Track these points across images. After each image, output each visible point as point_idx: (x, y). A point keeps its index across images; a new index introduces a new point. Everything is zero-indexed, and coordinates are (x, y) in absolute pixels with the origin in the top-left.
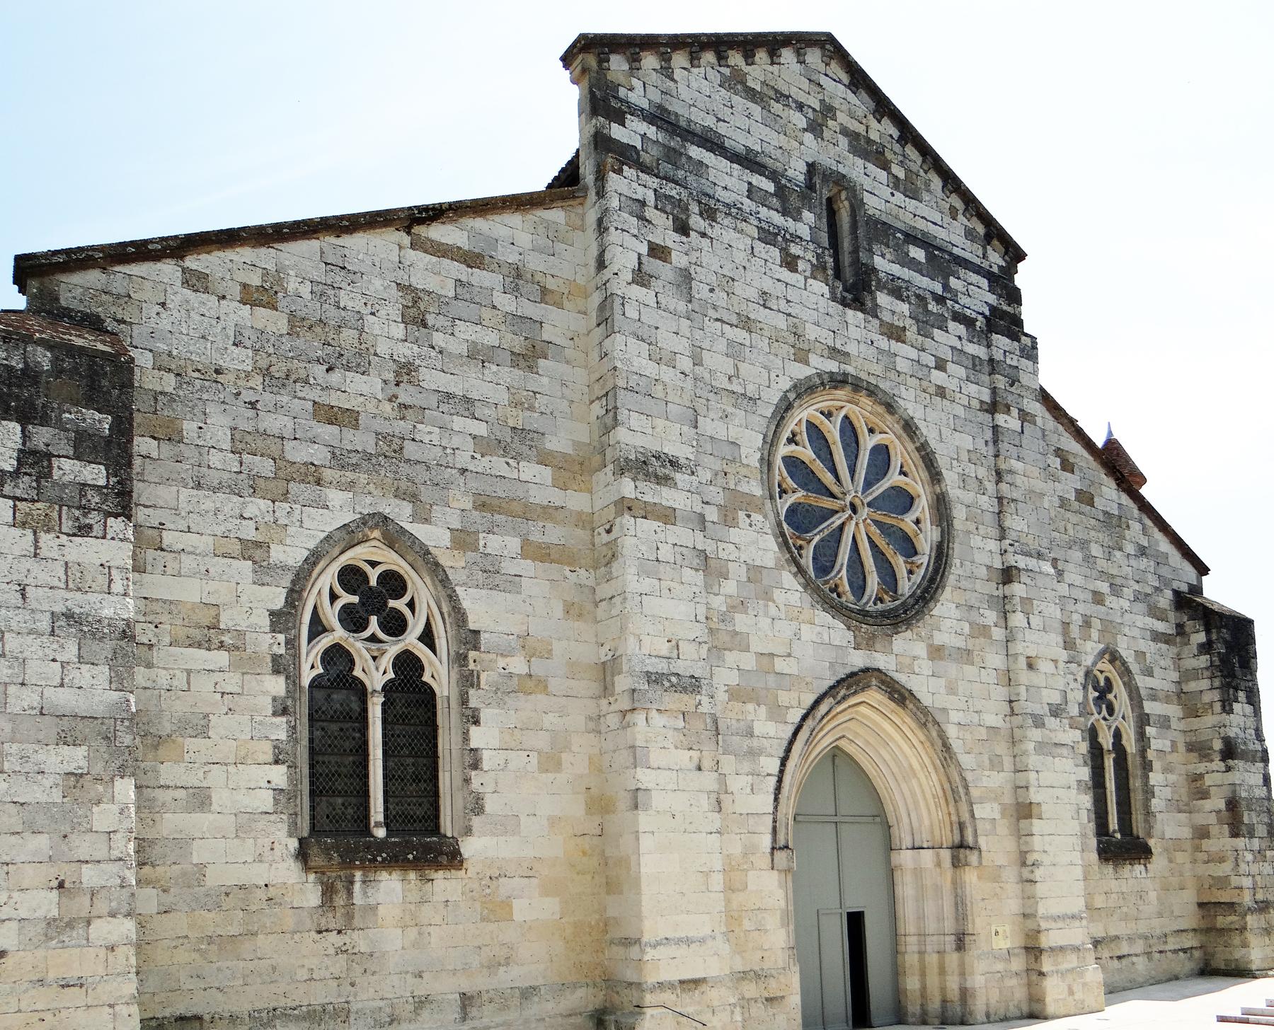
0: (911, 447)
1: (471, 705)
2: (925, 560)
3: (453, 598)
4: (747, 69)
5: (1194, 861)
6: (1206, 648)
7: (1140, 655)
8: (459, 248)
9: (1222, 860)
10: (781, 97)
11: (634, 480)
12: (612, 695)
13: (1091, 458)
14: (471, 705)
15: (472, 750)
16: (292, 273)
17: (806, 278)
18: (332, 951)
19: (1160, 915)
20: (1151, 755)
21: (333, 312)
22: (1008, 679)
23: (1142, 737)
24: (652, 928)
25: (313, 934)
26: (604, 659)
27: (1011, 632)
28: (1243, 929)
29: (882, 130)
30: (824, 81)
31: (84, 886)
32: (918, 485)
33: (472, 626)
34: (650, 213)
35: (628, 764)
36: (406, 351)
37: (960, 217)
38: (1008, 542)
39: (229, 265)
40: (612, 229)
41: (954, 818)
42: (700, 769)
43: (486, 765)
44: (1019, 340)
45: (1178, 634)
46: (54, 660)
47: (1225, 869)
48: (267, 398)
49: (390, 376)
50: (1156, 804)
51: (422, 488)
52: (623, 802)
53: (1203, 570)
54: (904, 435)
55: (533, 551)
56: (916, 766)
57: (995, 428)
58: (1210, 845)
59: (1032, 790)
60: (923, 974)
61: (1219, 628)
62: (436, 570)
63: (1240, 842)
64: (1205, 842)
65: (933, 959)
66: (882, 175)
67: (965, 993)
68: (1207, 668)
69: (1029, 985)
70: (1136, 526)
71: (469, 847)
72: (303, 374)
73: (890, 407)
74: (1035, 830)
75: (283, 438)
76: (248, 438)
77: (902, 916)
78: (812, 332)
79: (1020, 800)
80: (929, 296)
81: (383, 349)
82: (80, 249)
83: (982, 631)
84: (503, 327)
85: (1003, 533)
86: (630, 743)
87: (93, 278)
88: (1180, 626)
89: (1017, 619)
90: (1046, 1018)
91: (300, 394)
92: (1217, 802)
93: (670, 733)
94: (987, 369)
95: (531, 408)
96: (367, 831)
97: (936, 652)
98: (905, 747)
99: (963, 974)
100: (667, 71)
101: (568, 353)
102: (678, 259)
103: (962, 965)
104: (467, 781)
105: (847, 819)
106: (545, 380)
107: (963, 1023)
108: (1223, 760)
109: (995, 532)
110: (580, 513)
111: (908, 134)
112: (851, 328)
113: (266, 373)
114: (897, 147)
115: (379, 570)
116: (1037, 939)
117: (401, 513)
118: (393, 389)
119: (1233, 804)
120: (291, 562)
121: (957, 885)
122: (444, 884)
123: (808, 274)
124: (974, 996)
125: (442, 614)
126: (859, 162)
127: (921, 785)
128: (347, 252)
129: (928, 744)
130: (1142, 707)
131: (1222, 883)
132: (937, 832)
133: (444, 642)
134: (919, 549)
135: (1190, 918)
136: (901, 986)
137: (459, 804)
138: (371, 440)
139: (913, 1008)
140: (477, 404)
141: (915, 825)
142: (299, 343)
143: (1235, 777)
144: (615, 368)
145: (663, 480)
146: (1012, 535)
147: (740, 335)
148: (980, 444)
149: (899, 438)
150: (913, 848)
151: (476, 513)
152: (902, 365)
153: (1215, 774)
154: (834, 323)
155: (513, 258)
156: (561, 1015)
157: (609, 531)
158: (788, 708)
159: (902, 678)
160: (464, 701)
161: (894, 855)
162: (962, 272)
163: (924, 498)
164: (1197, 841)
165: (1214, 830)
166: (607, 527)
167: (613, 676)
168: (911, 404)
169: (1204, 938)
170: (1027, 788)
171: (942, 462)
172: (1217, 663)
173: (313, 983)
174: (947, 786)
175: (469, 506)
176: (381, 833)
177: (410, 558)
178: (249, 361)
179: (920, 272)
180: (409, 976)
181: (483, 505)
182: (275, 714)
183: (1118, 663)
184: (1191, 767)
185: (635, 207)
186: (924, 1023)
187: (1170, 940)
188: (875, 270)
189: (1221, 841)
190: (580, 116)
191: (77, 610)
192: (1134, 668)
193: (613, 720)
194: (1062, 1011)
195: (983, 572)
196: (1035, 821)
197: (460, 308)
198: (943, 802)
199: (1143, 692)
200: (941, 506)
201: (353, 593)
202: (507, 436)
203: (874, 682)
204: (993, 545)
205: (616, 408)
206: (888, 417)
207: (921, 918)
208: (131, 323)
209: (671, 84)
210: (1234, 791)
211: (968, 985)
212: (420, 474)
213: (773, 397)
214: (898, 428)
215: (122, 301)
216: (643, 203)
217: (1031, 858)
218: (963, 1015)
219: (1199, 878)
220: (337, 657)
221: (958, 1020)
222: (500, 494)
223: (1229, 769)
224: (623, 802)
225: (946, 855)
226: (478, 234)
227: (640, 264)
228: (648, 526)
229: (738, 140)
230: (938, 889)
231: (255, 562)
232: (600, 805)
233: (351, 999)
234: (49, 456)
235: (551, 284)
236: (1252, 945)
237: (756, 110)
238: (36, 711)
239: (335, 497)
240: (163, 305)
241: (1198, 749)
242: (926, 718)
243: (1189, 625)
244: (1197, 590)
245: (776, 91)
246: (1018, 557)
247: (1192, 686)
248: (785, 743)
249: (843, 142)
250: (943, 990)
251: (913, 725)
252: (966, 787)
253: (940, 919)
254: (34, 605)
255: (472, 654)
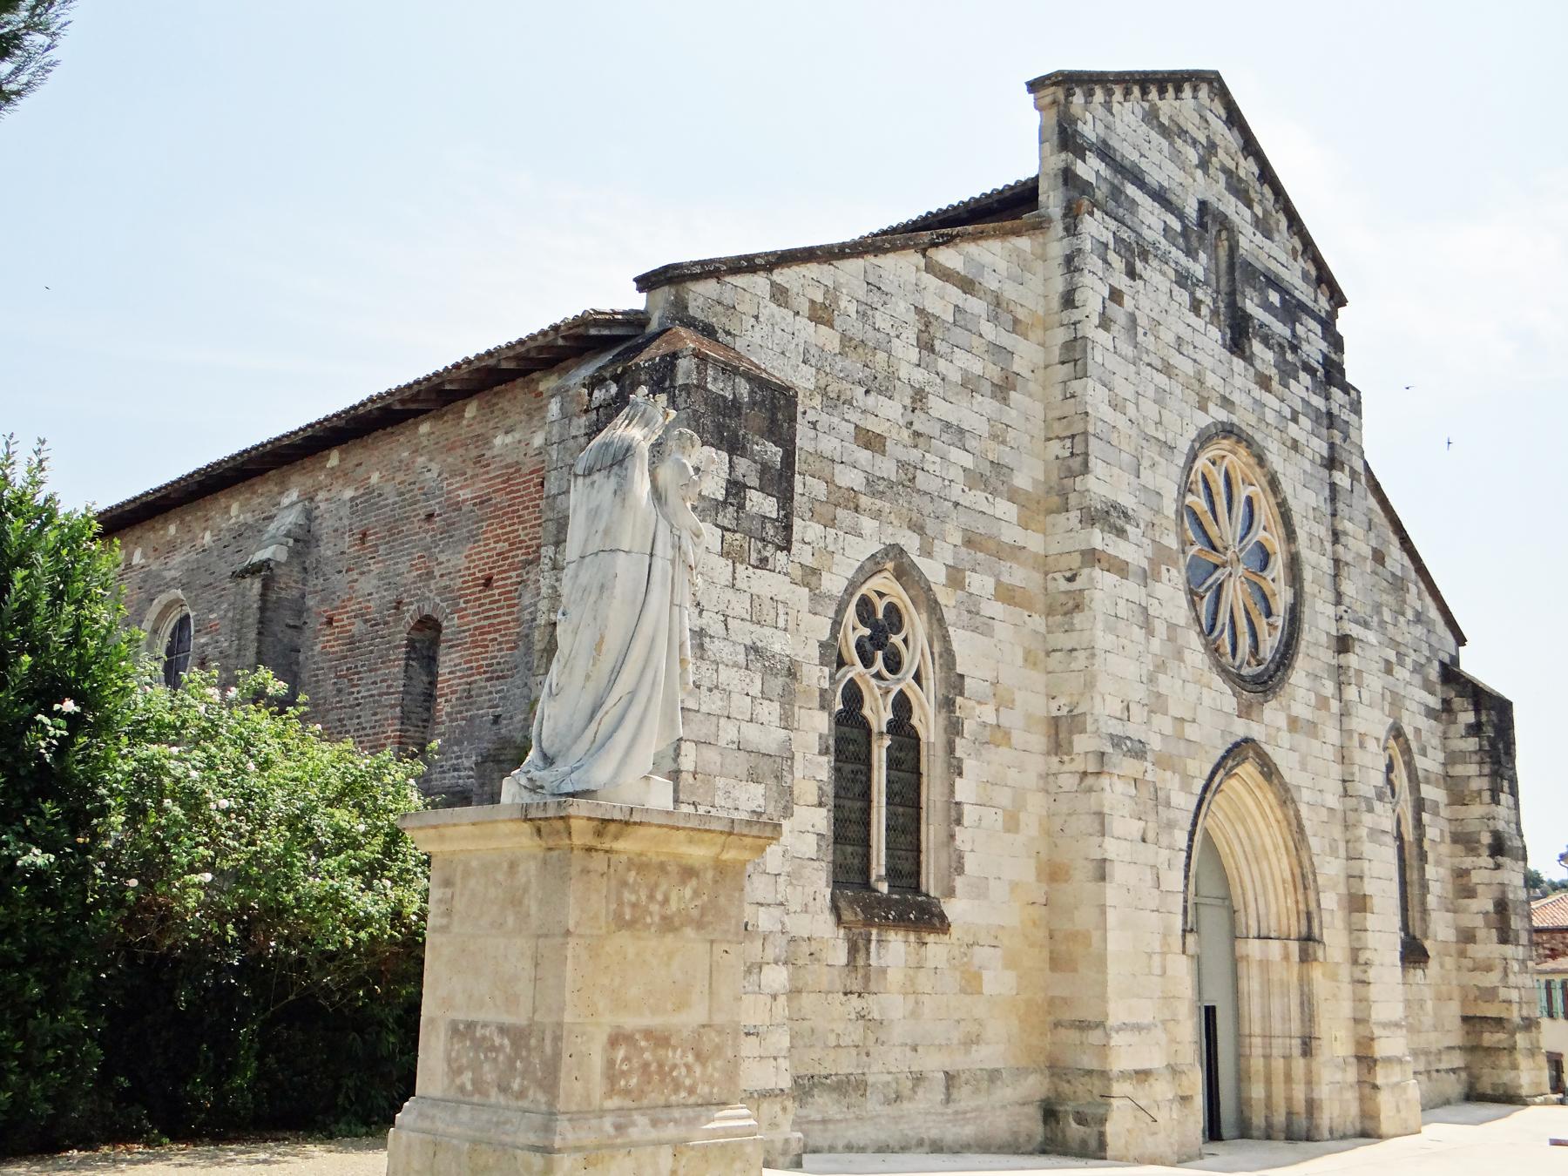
0: (1272, 501)
1: (957, 755)
2: (1280, 623)
3: (946, 639)
4: (1160, 103)
5: (1459, 968)
6: (1475, 729)
7: (1418, 731)
8: (958, 273)
9: (1489, 969)
10: (1183, 133)
11: (1102, 531)
12: (1069, 753)
13: (1382, 514)
14: (957, 755)
15: (956, 803)
16: (844, 291)
17: (1206, 323)
18: (853, 1016)
19: (1435, 1028)
20: (1427, 845)
21: (871, 333)
22: (1343, 758)
23: (1419, 824)
24: (1117, 1013)
25: (841, 994)
26: (1055, 713)
27: (1346, 705)
28: (1512, 1049)
29: (1248, 168)
30: (1210, 116)
31: (760, 929)
32: (1276, 544)
33: (959, 670)
34: (1112, 257)
35: (1091, 831)
36: (919, 376)
37: (1299, 258)
38: (1343, 608)
39: (802, 281)
40: (1086, 272)
41: (1302, 907)
42: (1144, 840)
43: (966, 821)
44: (1349, 394)
45: (1444, 710)
46: (747, 694)
47: (1492, 979)
48: (824, 419)
49: (908, 402)
50: (1431, 900)
51: (928, 520)
52: (1082, 872)
53: (1461, 640)
54: (1268, 489)
55: (1006, 594)
56: (1270, 847)
57: (1333, 486)
58: (1473, 950)
59: (1366, 880)
60: (1268, 1081)
61: (1488, 709)
62: (933, 608)
63: (1509, 950)
64: (1470, 947)
65: (1278, 1065)
66: (1247, 213)
67: (1311, 1105)
68: (1475, 752)
69: (1362, 1099)
70: (1413, 589)
71: (953, 909)
72: (848, 395)
73: (1261, 461)
74: (1369, 925)
75: (833, 461)
76: (811, 459)
77: (1246, 1014)
78: (1212, 380)
79: (1353, 891)
80: (1286, 344)
81: (903, 374)
82: (712, 261)
83: (1323, 703)
84: (986, 357)
85: (1339, 599)
86: (1094, 808)
87: (708, 288)
88: (1446, 703)
89: (1351, 693)
90: (1380, 1137)
91: (847, 417)
92: (1485, 903)
93: (1128, 801)
94: (1325, 422)
95: (1004, 442)
96: (867, 885)
97: (1293, 723)
98: (1262, 825)
99: (1309, 1083)
100: (1108, 106)
101: (1032, 386)
102: (1128, 302)
103: (1309, 1071)
104: (952, 837)
105: (1208, 901)
106: (1014, 413)
107: (1309, 1139)
108: (1492, 855)
109: (1331, 596)
110: (1036, 555)
111: (1267, 174)
112: (1236, 376)
113: (824, 391)
114: (1257, 185)
115: (886, 600)
116: (1370, 1047)
117: (910, 542)
118: (910, 416)
119: (1502, 906)
120: (835, 592)
121: (1305, 984)
122: (937, 948)
123: (1207, 319)
124: (1320, 1108)
125: (932, 653)
126: (1233, 199)
127: (1271, 868)
128: (881, 272)
129: (1284, 824)
130: (1419, 790)
131: (1489, 994)
132: (1284, 921)
133: (932, 683)
134: (1274, 610)
135: (1455, 1035)
136: (1244, 1095)
137: (944, 861)
138: (893, 466)
139: (1258, 1120)
140: (967, 435)
141: (1262, 911)
142: (847, 363)
143: (1501, 876)
144: (1086, 413)
145: (1121, 533)
146: (1346, 600)
147: (1161, 379)
148: (1322, 504)
149: (1264, 491)
150: (1259, 937)
151: (964, 549)
152: (1270, 417)
153: (1483, 871)
154: (1223, 370)
155: (994, 286)
156: (1017, 1103)
157: (1071, 579)
158: (1193, 777)
159: (1268, 749)
160: (951, 748)
161: (1240, 944)
162: (1305, 318)
163: (1279, 555)
164: (1462, 946)
165: (1481, 934)
166: (1068, 574)
167: (1071, 733)
168: (1275, 459)
169: (1469, 1058)
170: (1361, 878)
171: (1297, 519)
172: (1487, 748)
173: (840, 1050)
174: (1297, 871)
175: (959, 541)
176: (884, 888)
177: (913, 592)
178: (813, 380)
179: (1275, 316)
180: (908, 1049)
181: (969, 542)
182: (820, 753)
183: (1401, 739)
184: (1456, 861)
185: (1102, 249)
186: (1269, 1137)
187: (1444, 1057)
188: (1250, 317)
189: (1487, 947)
190: (1041, 142)
191: (759, 644)
192: (1414, 746)
193: (1068, 782)
194: (1392, 1132)
195: (1323, 639)
196: (1369, 915)
197: (959, 335)
198: (1291, 889)
199: (1421, 774)
200: (1294, 563)
202: (986, 469)
203: (1251, 754)
204: (1330, 610)
205: (1086, 454)
206: (1258, 469)
207: (1267, 1016)
208: (735, 335)
209: (1111, 118)
210: (1504, 893)
211: (1315, 1096)
212: (928, 508)
213: (1184, 446)
214: (1264, 481)
215: (729, 313)
216: (1106, 246)
217: (1362, 958)
218: (1309, 1130)
219: (1462, 987)
221: (1304, 1134)
222: (982, 531)
223: (1498, 867)
224: (1082, 872)
225: (1294, 947)
226: (969, 260)
227: (1104, 307)
228: (1110, 579)
229: (1155, 177)
230: (1284, 985)
231: (811, 590)
232: (1054, 873)
233: (866, 1070)
234: (745, 486)
235: (1021, 314)
236: (1521, 1067)
237: (1165, 144)
238: (735, 746)
239: (868, 524)
240: (756, 317)
241: (1464, 840)
242: (1286, 797)
243: (1458, 702)
244: (1455, 660)
245: (1179, 127)
246: (1353, 625)
247: (1459, 770)
248: (1191, 816)
249: (1222, 178)
250: (1289, 1100)
251: (1274, 802)
252: (1314, 874)
253: (1286, 1019)
254: (733, 638)
255: (959, 700)
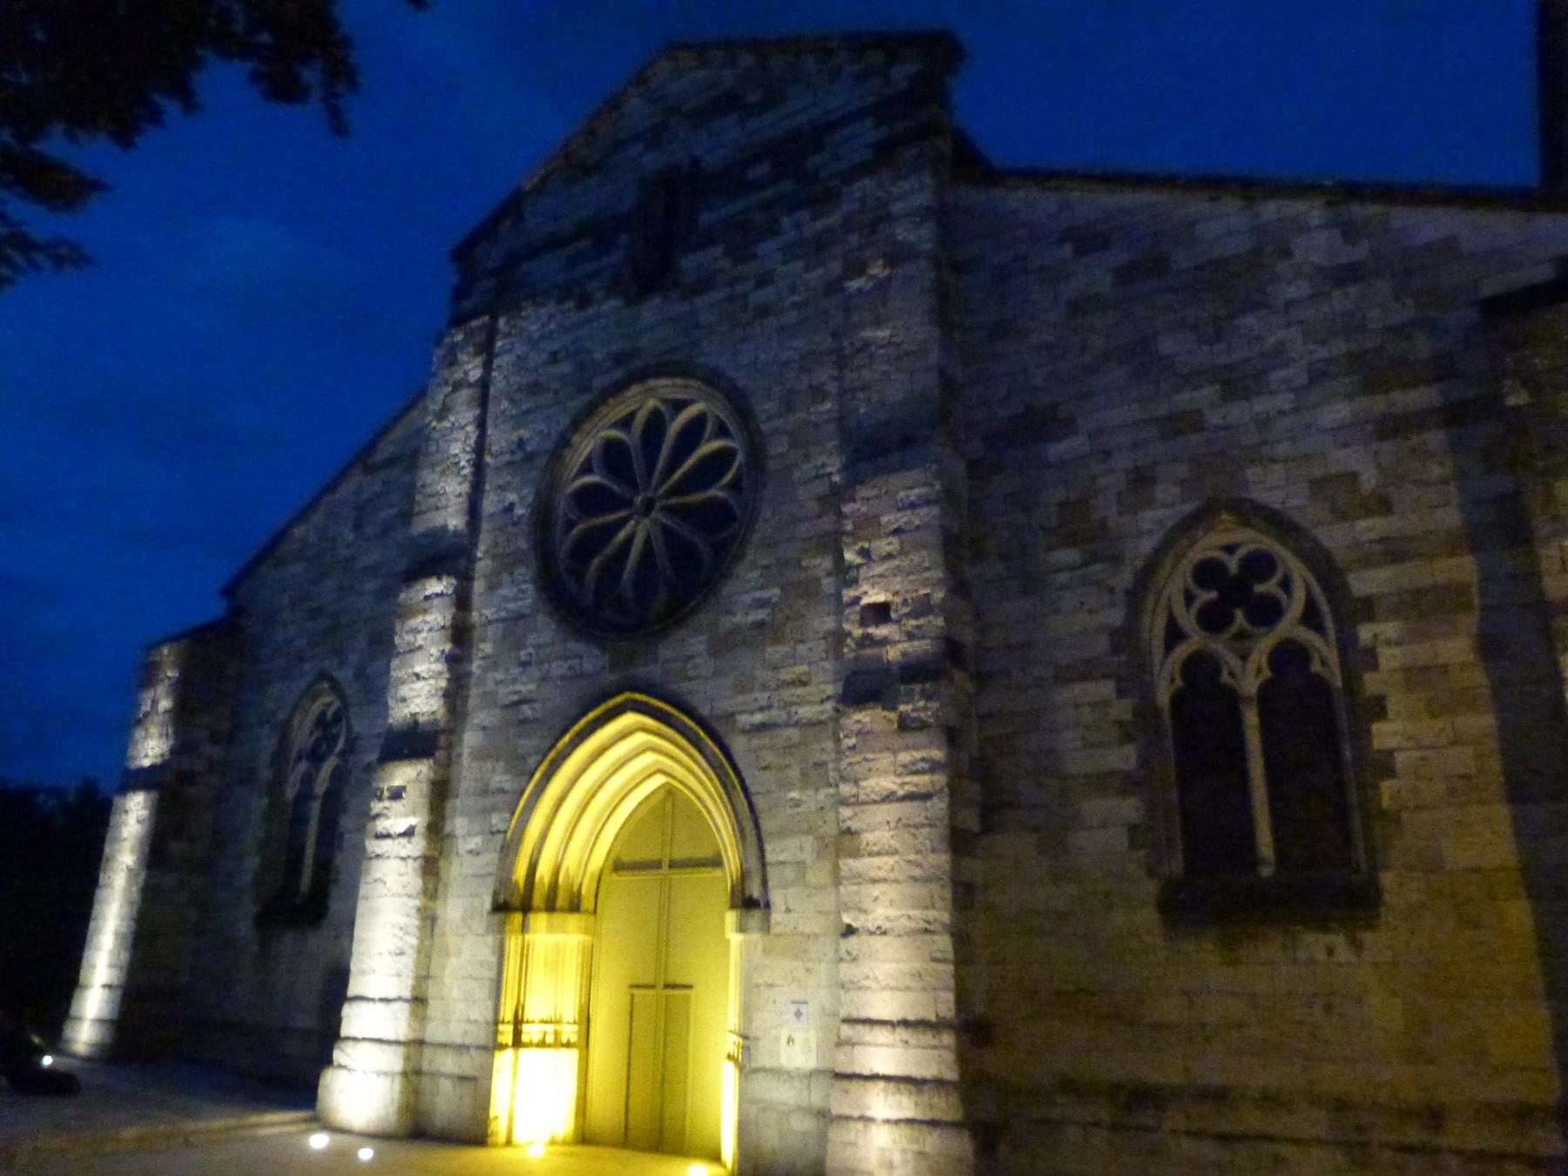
201: (1209, 589)
220: (1200, 669)
